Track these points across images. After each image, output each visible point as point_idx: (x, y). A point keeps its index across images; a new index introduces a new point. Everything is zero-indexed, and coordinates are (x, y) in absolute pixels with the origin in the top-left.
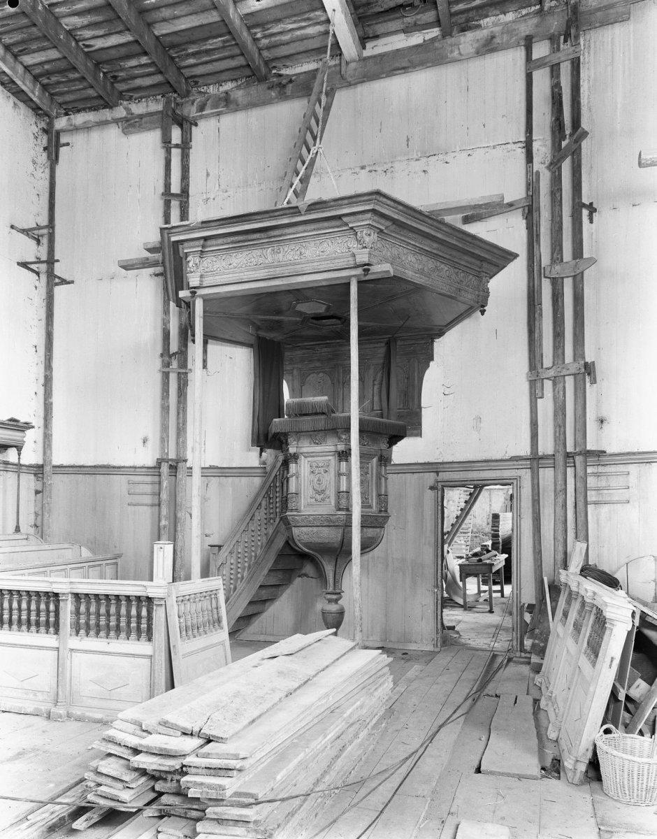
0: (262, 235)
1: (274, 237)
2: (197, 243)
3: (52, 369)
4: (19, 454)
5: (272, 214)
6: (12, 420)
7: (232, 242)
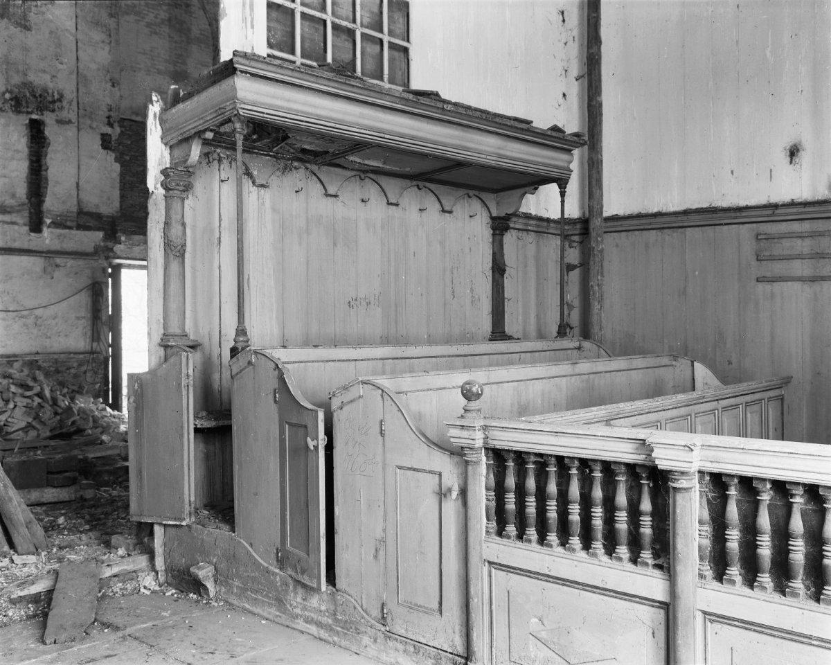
3: (601, 42)
4: (563, 194)
6: (555, 129)
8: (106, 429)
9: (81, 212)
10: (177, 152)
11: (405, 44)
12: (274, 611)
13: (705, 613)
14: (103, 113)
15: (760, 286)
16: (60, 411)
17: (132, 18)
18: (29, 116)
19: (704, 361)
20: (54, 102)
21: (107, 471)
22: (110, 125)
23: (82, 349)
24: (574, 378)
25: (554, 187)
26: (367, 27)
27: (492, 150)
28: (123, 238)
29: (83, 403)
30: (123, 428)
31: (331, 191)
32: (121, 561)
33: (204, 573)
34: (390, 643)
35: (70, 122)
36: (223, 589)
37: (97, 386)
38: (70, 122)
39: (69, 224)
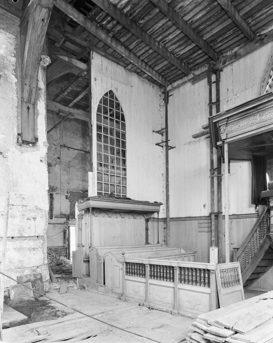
0: (254, 110)
1: (260, 109)
2: (224, 120)
5: (259, 99)
7: (240, 116)
8: (67, 264)
9: (61, 214)
10: (81, 212)
11: (125, 186)
12: (96, 291)
13: (150, 283)
14: (66, 191)
15: (199, 233)
16: (57, 260)
17: (73, 168)
18: (50, 193)
19: (183, 248)
20: (55, 189)
21: (68, 272)
22: (68, 193)
23: (61, 246)
24: (152, 252)
25: (156, 213)
26: (118, 184)
27: (141, 208)
28: (71, 220)
29: (62, 258)
30: (71, 264)
31: (110, 216)
32: (71, 284)
33: (85, 285)
34: (113, 294)
35: (59, 193)
36: (88, 288)
37: (65, 254)
38: (59, 193)
39: (58, 217)
